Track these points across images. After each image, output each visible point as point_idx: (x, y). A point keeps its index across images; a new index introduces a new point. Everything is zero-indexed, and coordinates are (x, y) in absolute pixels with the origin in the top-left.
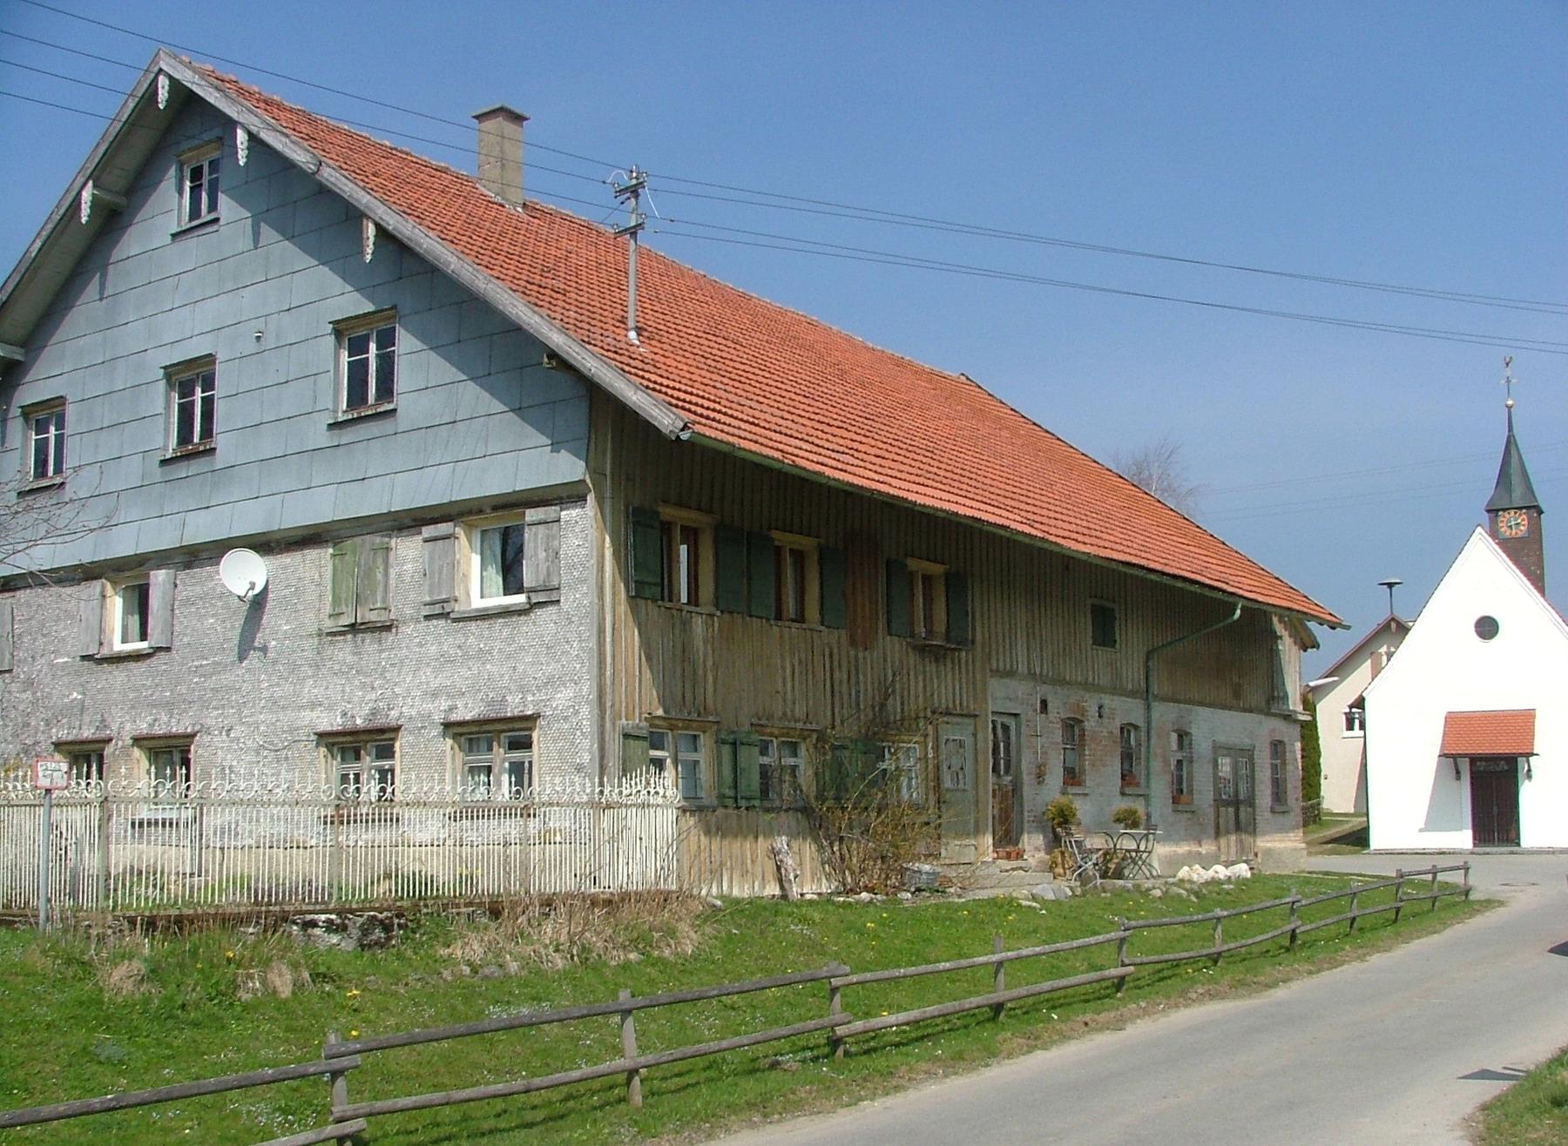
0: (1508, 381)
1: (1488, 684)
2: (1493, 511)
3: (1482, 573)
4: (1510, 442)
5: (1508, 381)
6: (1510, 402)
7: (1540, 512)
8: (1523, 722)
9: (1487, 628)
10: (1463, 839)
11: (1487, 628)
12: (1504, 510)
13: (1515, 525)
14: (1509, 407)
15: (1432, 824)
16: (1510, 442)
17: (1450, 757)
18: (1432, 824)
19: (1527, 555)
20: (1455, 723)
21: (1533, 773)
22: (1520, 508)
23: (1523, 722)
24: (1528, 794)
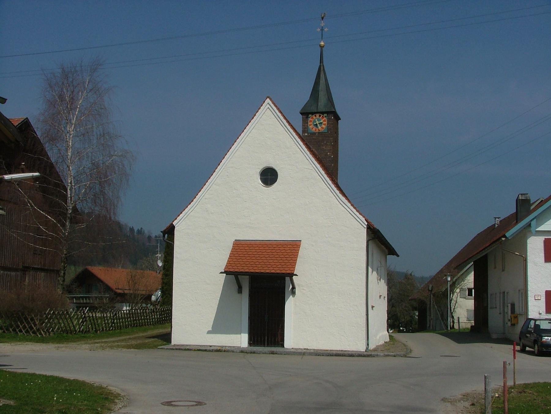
0: (322, 30)
1: (264, 218)
2: (306, 114)
3: (270, 135)
4: (321, 70)
5: (322, 30)
6: (322, 43)
7: (337, 118)
8: (290, 250)
9: (269, 176)
10: (242, 340)
11: (269, 176)
12: (313, 113)
13: (319, 124)
14: (322, 47)
15: (217, 328)
16: (321, 70)
17: (233, 274)
18: (218, 327)
19: (324, 149)
20: (241, 248)
21: (297, 291)
22: (323, 113)
23: (290, 250)
24: (291, 306)
